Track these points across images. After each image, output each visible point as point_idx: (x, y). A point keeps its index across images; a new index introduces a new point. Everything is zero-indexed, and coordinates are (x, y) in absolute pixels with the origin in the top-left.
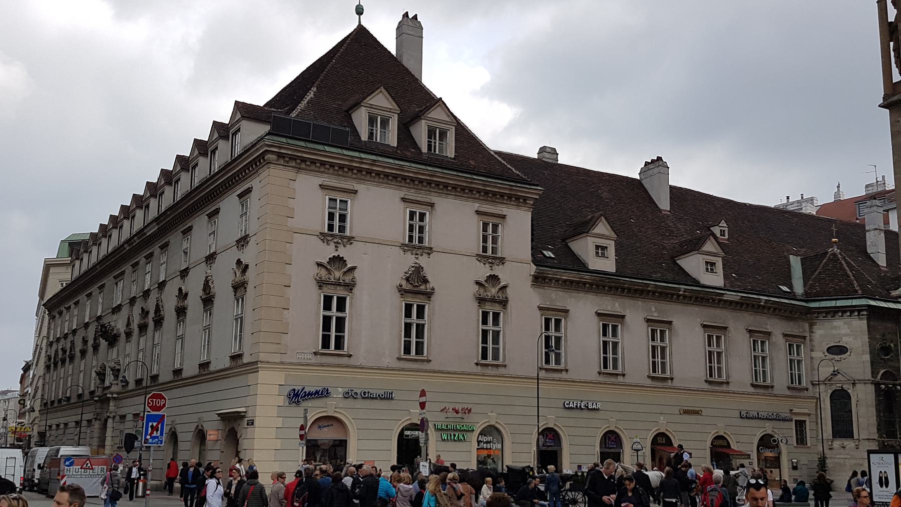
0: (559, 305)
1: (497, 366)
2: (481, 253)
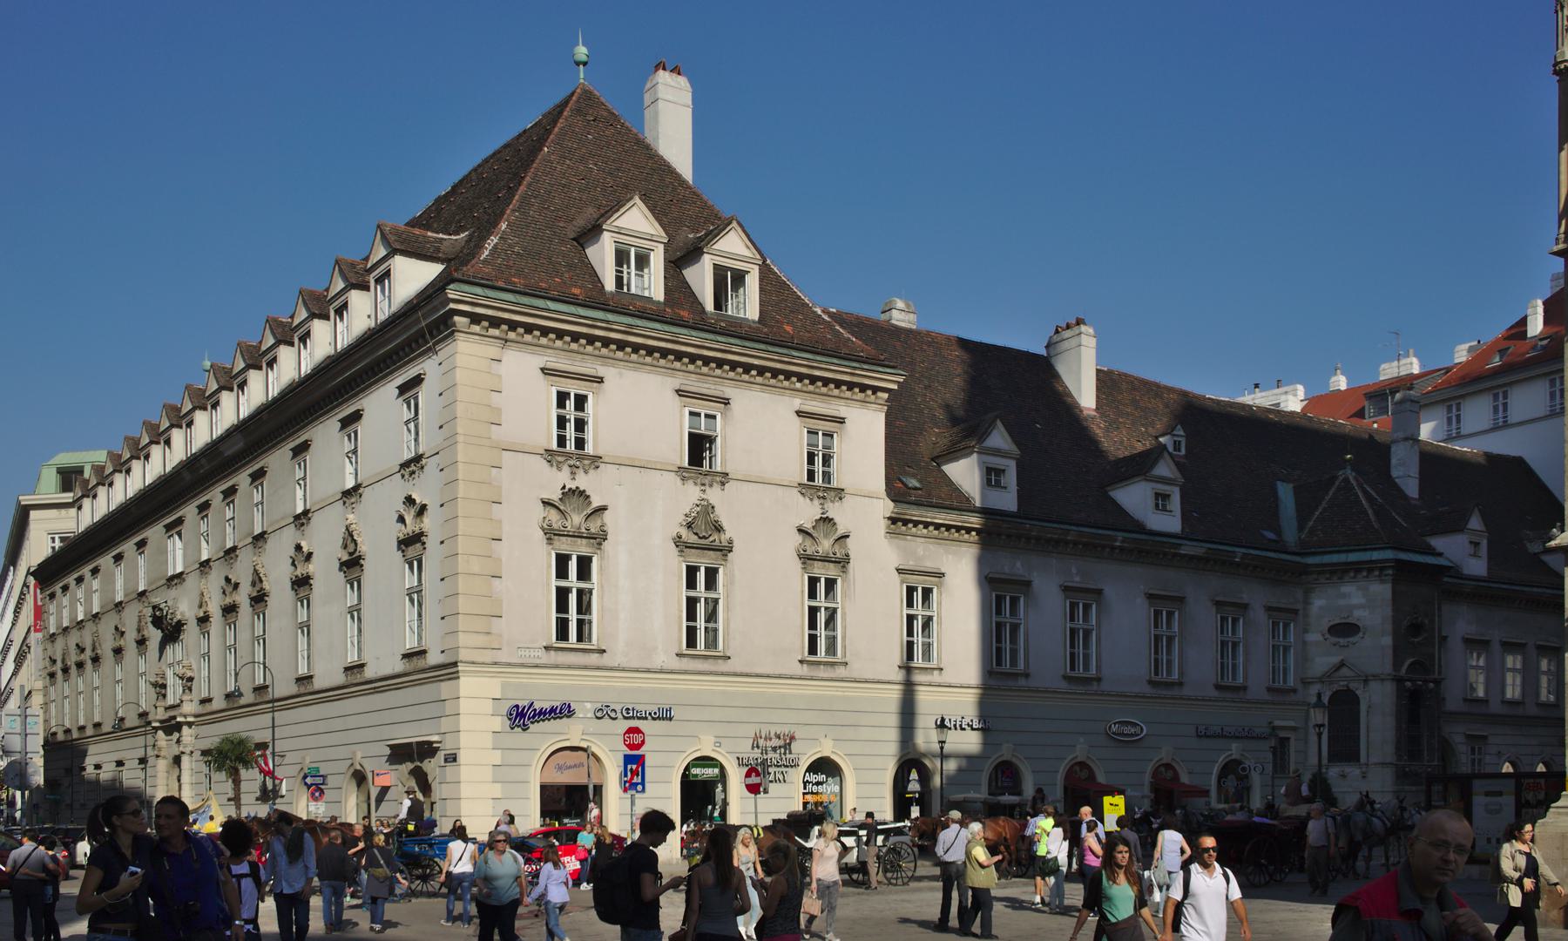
0: (929, 565)
1: (833, 664)
2: (806, 482)
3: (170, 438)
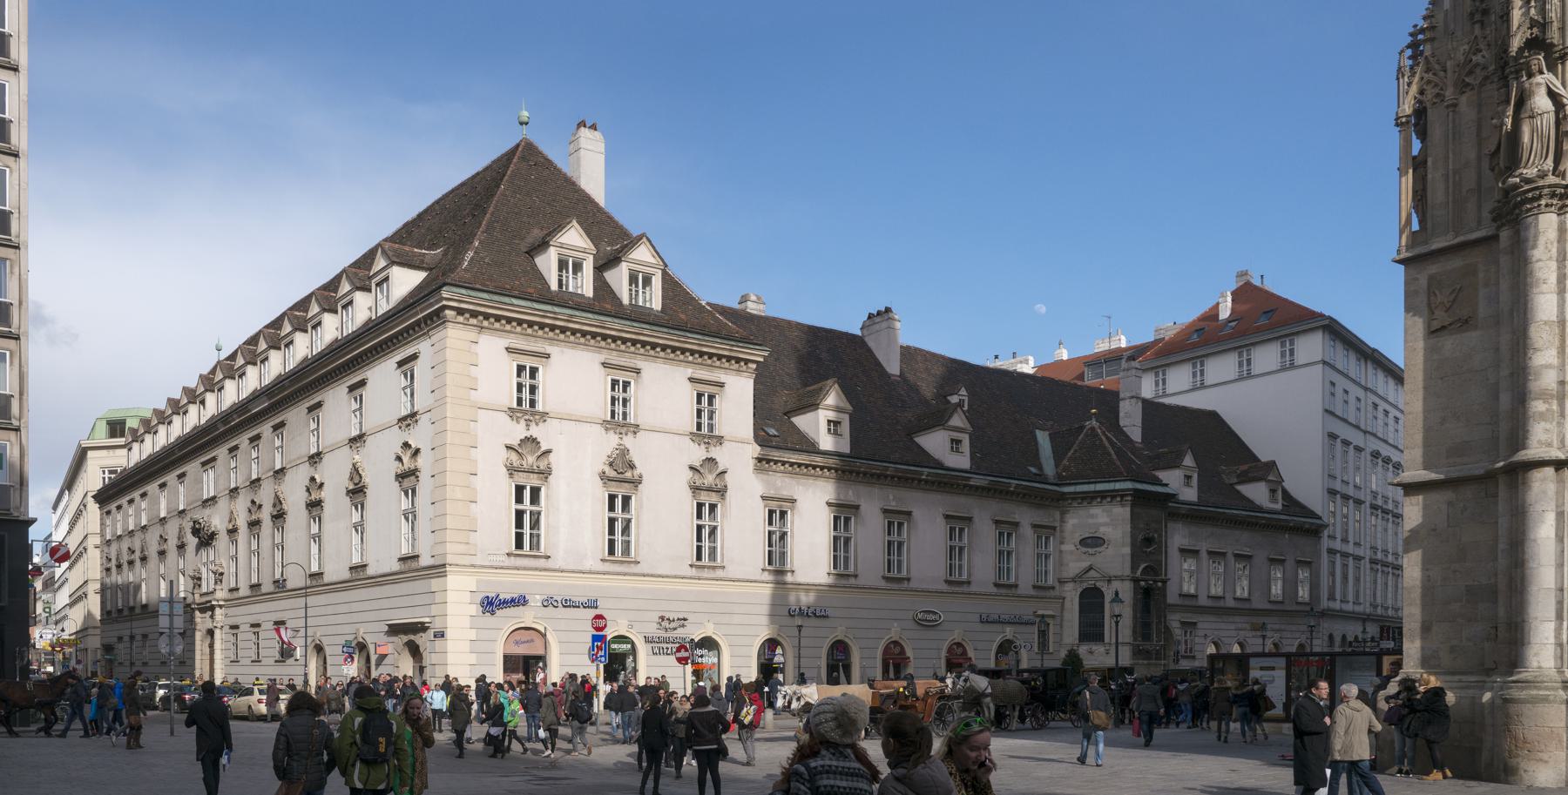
0: (785, 493)
3: (204, 400)
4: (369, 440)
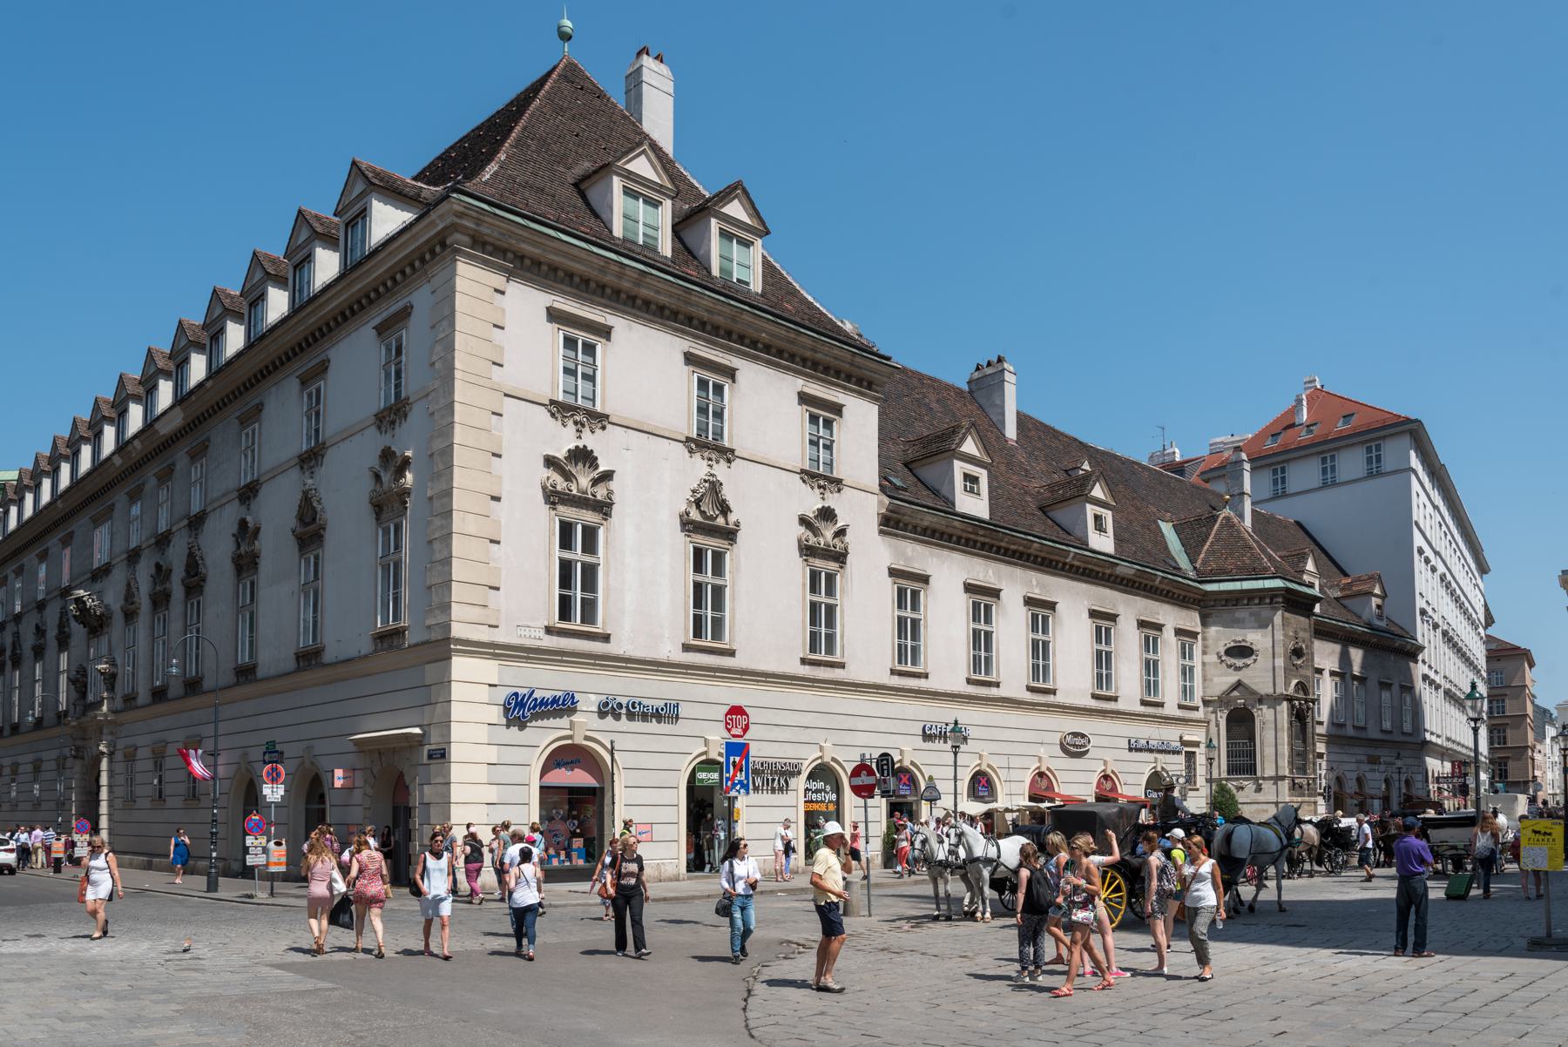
0: (917, 567)
4: (330, 455)
